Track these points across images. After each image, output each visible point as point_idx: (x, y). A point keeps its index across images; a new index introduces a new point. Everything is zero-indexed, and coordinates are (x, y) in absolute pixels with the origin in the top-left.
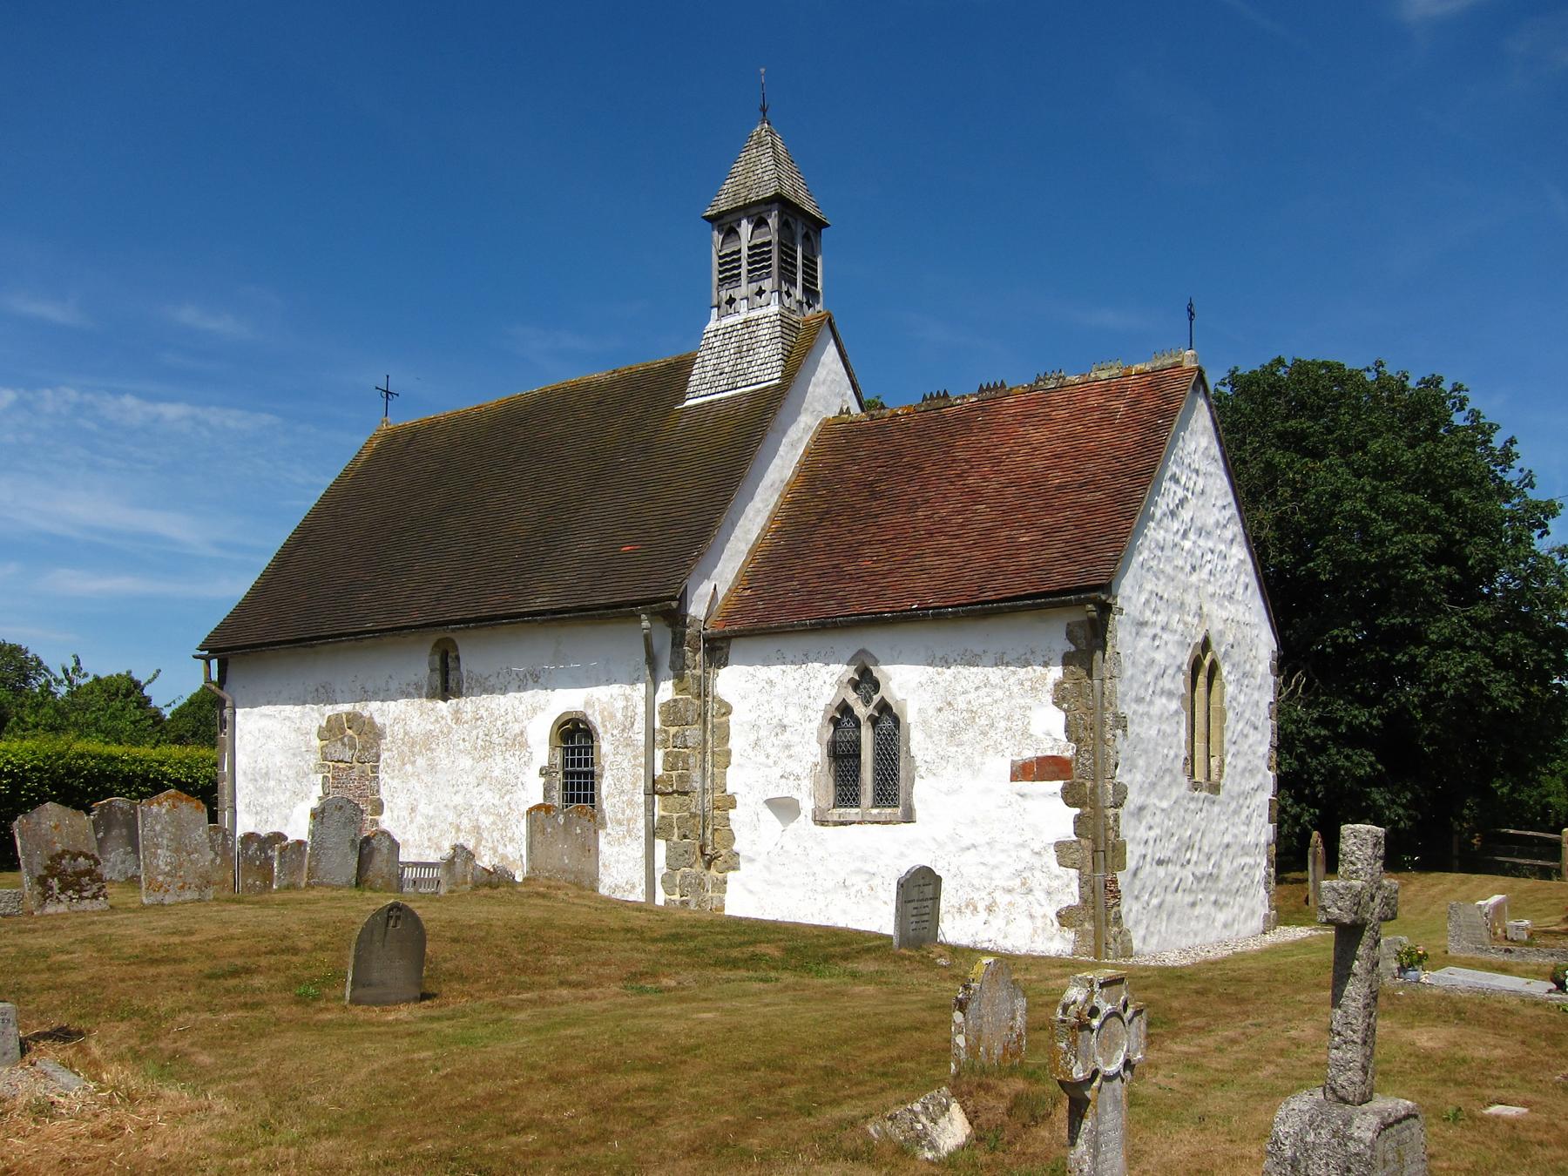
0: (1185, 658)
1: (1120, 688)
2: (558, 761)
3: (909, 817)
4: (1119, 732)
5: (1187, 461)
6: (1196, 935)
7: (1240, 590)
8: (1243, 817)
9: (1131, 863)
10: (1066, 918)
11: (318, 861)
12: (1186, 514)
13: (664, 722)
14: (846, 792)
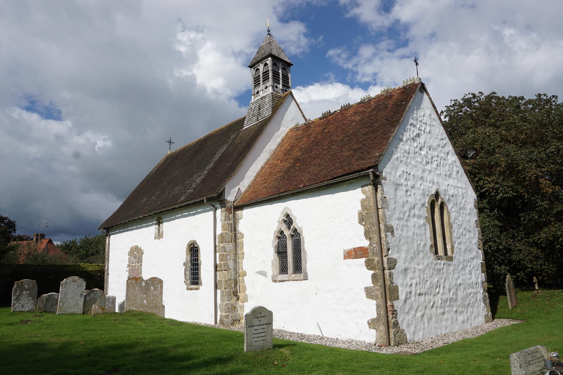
0: (427, 200)
1: (388, 213)
2: (189, 259)
3: (306, 278)
4: (389, 234)
5: (420, 119)
6: (446, 328)
7: (454, 173)
8: (467, 271)
9: (402, 297)
10: (372, 324)
11: (64, 303)
12: (422, 140)
13: (219, 242)
14: (283, 269)
